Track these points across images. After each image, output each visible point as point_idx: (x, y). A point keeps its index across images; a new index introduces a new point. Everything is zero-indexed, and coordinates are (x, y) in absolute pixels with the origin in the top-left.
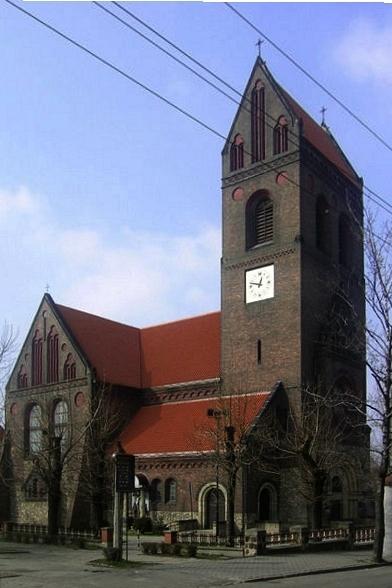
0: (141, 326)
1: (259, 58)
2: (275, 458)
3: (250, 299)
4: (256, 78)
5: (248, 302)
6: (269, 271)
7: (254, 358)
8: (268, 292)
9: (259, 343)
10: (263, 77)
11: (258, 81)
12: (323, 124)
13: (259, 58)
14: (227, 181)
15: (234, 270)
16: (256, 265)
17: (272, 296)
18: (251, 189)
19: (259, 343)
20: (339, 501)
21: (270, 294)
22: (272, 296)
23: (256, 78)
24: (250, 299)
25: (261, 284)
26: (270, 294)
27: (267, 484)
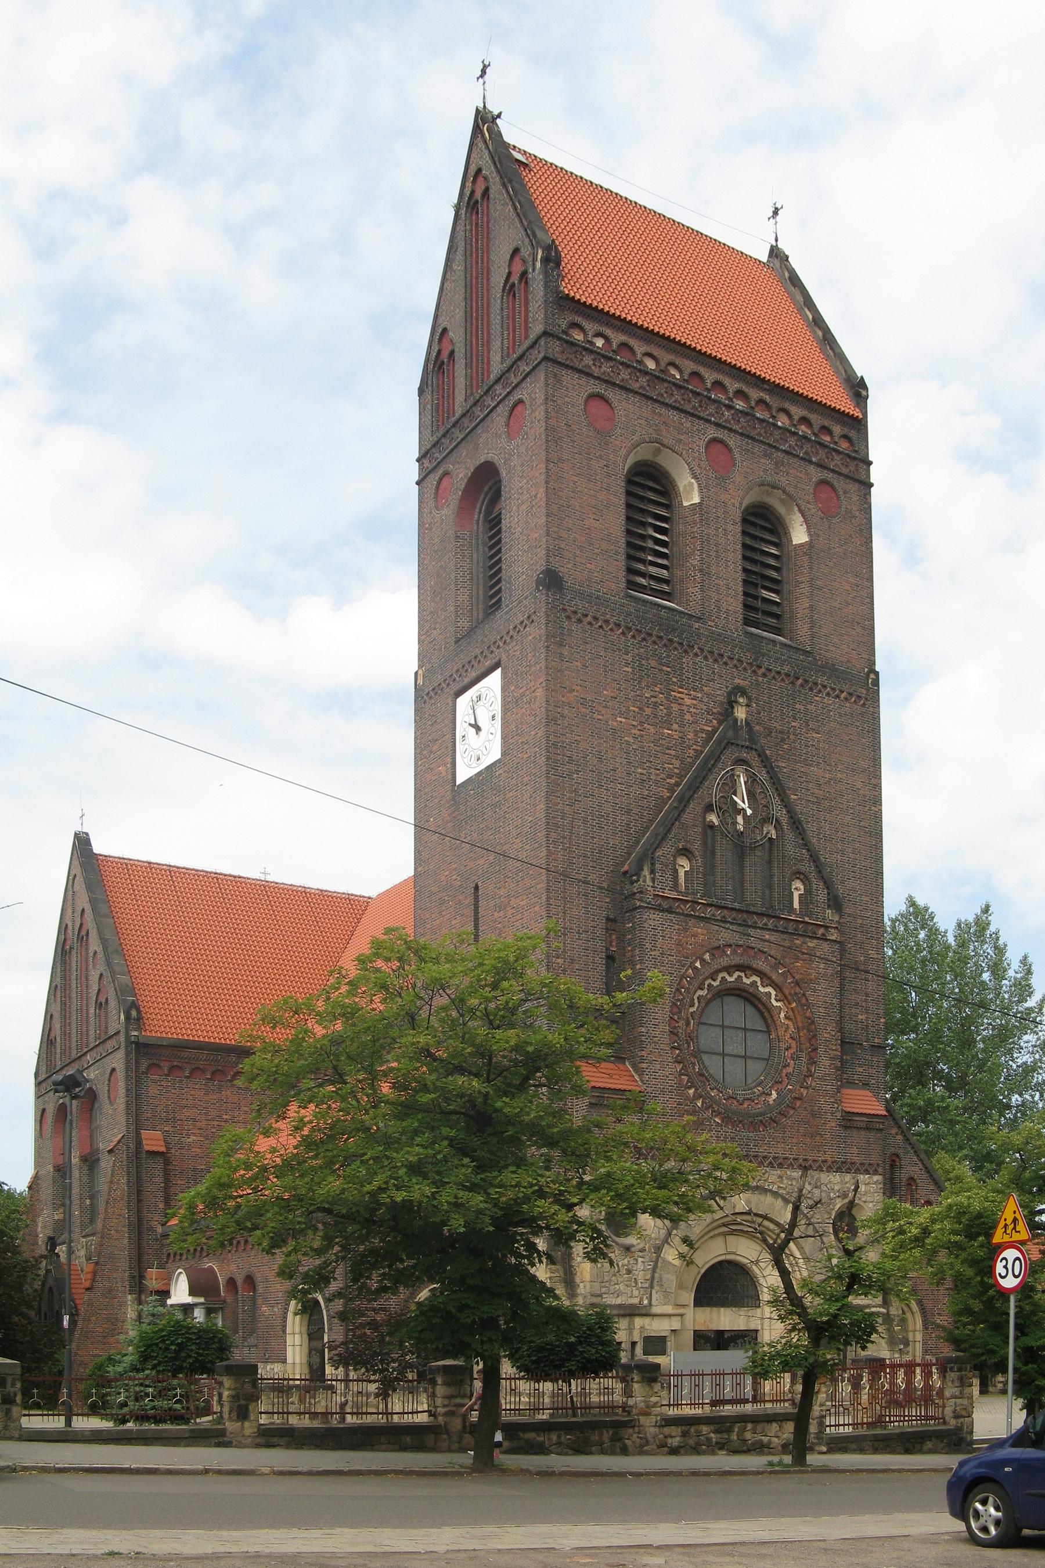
14: (426, 462)
16: (473, 674)
19: (476, 888)
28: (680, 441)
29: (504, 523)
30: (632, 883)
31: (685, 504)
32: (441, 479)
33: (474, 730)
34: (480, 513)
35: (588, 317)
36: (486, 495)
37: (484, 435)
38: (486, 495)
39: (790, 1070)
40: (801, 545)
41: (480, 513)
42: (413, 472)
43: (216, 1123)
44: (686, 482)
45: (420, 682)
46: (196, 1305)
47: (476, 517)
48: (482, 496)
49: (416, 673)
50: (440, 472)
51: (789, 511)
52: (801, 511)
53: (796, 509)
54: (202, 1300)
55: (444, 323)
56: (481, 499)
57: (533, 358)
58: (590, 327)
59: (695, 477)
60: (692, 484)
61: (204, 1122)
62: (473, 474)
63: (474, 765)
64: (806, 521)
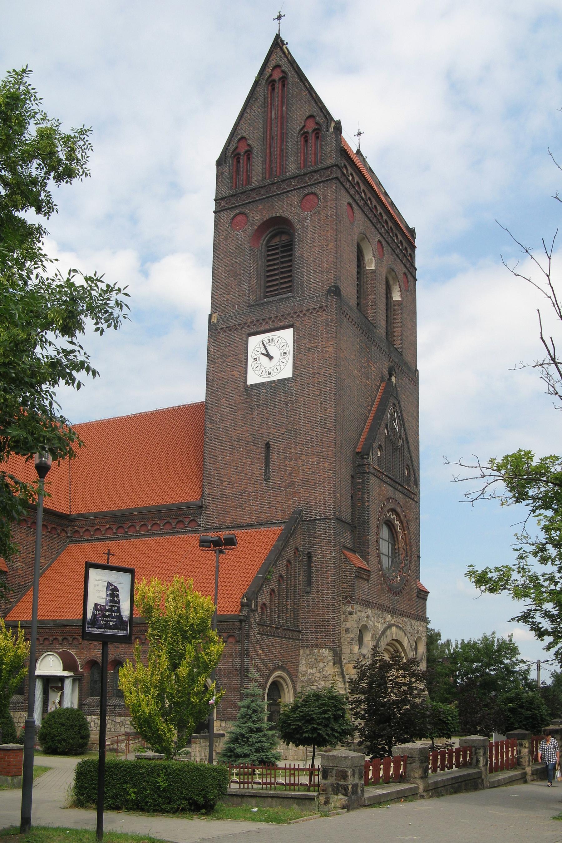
0: (428, 602)
1: (278, 37)
2: (315, 726)
3: (253, 378)
4: (272, 63)
5: (250, 382)
6: (287, 335)
7: (258, 469)
8: (285, 370)
9: (263, 344)
10: (284, 62)
11: (278, 66)
12: (358, 152)
13: (278, 37)
14: (223, 203)
15: (227, 335)
16: (267, 327)
17: (290, 375)
18: (258, 216)
19: (268, 446)
20: (232, 538)
21: (287, 372)
22: (290, 375)
23: (272, 63)
24: (253, 378)
25: (272, 357)
26: (287, 372)
27: (277, 673)
28: (371, 237)
29: (298, 252)
30: (363, 458)
31: (367, 268)
32: (236, 215)
33: (267, 359)
34: (264, 240)
35: (351, 166)
36: (270, 233)
37: (280, 203)
38: (270, 233)
39: (403, 565)
40: (397, 301)
41: (264, 240)
42: (212, 206)
43: (31, 555)
44: (369, 258)
45: (214, 320)
46: (68, 677)
47: (262, 242)
48: (268, 232)
49: (210, 316)
50: (237, 211)
51: (394, 283)
52: (399, 285)
53: (398, 283)
54: (72, 674)
55: (241, 133)
56: (266, 234)
57: (326, 174)
58: (350, 170)
59: (374, 257)
60: (372, 260)
61: (25, 555)
62: (268, 220)
63: (265, 376)
64: (401, 290)
